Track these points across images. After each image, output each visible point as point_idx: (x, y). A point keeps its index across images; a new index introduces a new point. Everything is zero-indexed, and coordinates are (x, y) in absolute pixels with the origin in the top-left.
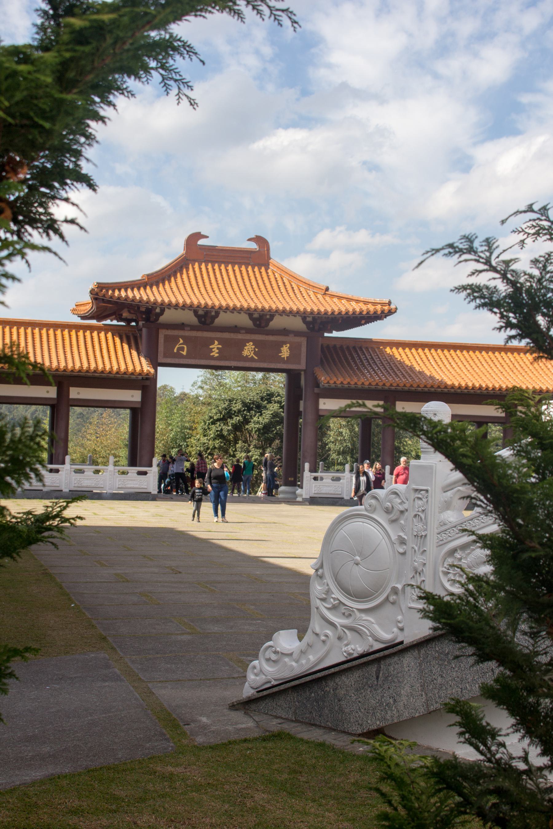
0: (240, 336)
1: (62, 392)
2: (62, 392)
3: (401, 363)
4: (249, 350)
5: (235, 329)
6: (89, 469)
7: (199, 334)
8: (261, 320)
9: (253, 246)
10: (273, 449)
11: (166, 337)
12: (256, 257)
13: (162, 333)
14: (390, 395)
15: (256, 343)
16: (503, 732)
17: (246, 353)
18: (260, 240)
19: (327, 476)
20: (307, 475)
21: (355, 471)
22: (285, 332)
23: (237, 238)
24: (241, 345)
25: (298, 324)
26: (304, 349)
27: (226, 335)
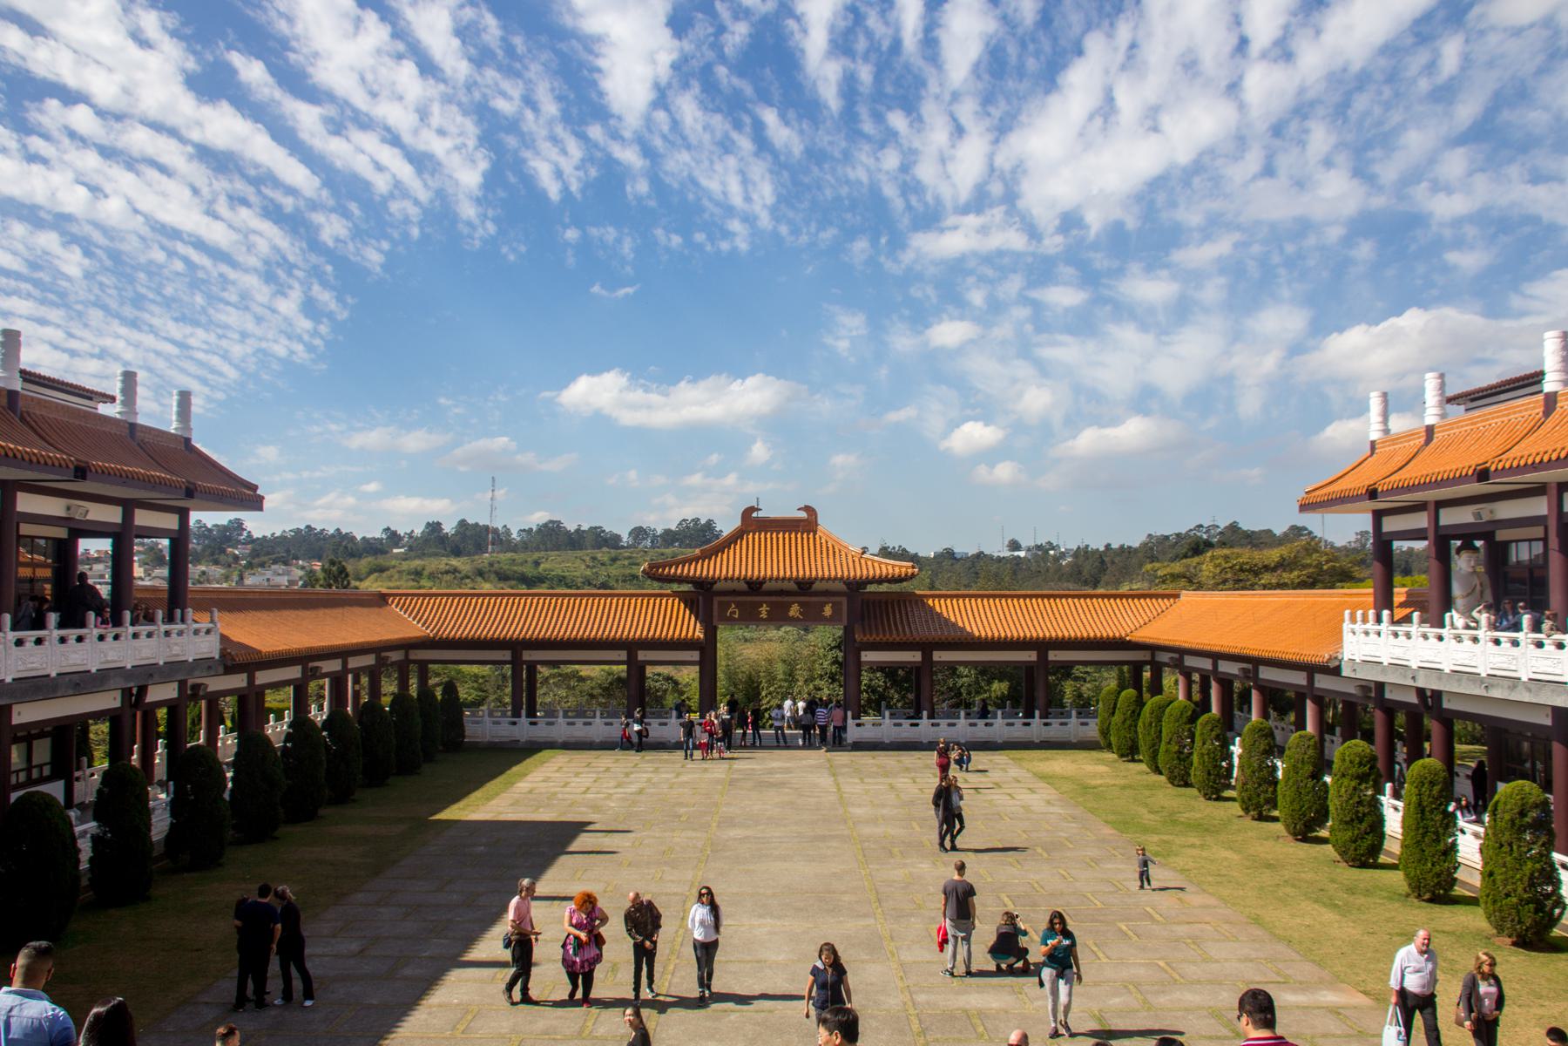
0: (786, 599)
1: (128, 516)
2: (128, 516)
3: (940, 615)
4: (794, 611)
5: (782, 593)
6: (579, 722)
7: (749, 599)
8: (804, 587)
9: (803, 515)
10: (374, 70)
11: (720, 603)
12: (806, 524)
13: (716, 600)
14: (927, 647)
15: (801, 604)
16: (1063, 987)
17: (791, 613)
18: (808, 509)
19: (1055, 722)
21: (1023, 701)
22: (826, 593)
23: (790, 510)
24: (788, 606)
25: (841, 587)
26: (845, 608)
27: (774, 599)
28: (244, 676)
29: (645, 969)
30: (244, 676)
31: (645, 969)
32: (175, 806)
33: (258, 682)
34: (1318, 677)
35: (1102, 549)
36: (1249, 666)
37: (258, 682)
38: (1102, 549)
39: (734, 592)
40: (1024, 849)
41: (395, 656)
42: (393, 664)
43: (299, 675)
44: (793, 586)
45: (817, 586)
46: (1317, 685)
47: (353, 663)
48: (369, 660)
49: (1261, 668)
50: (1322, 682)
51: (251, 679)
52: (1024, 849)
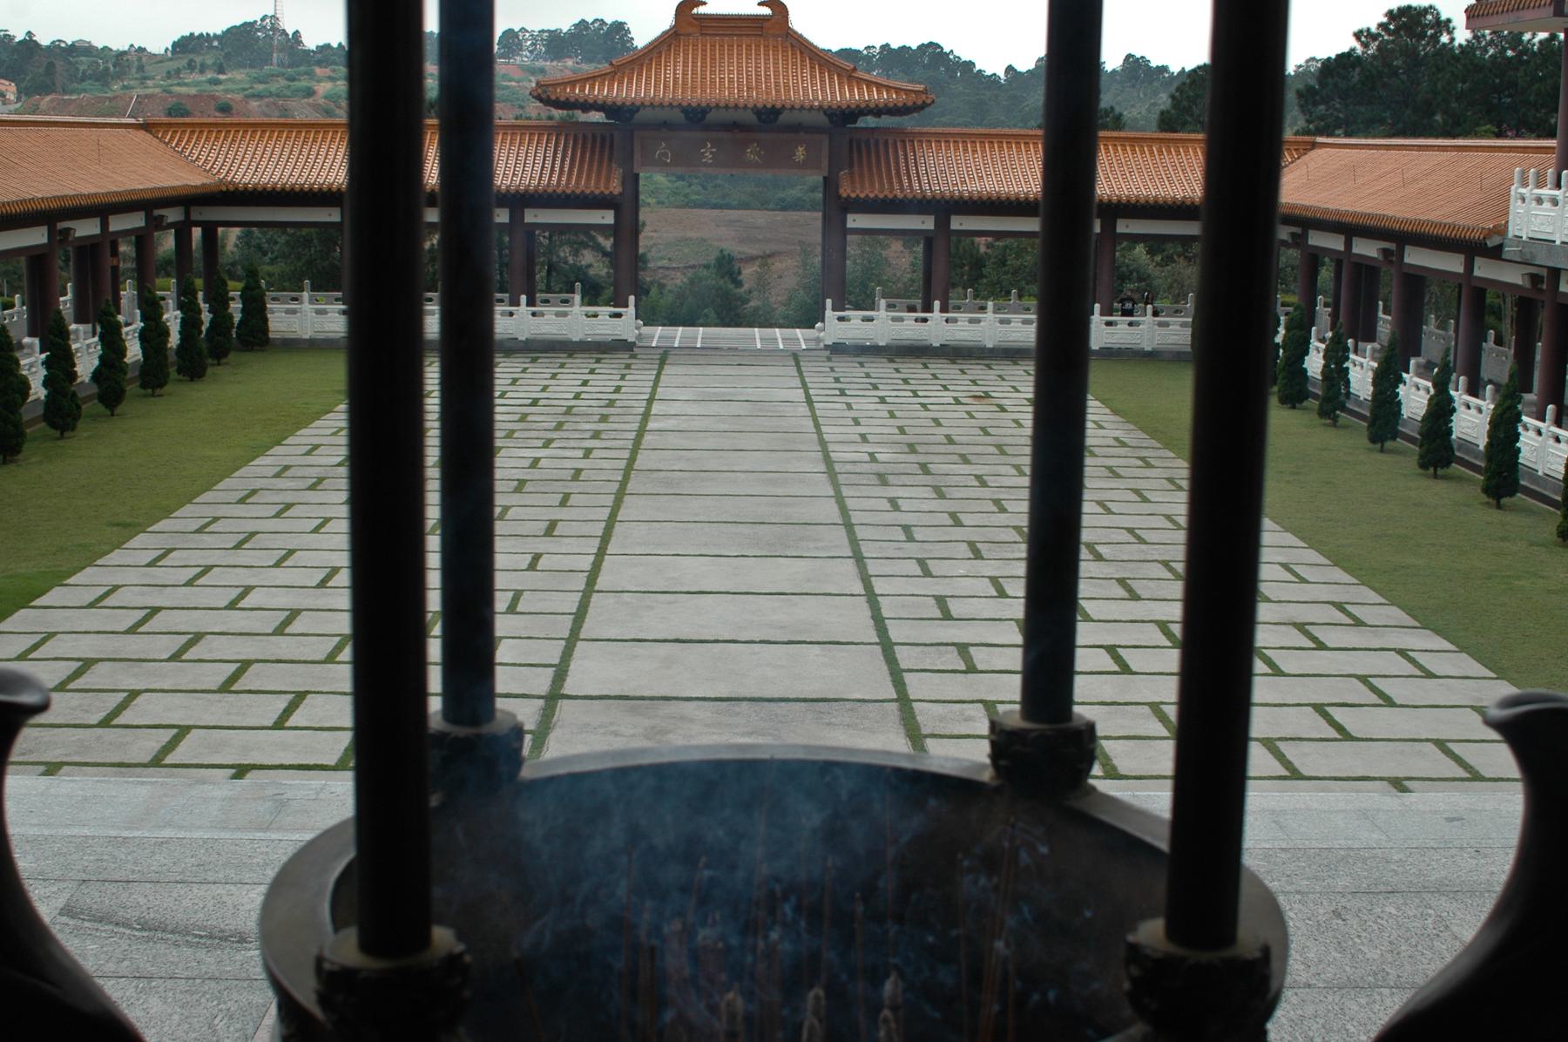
20: (830, 314)
22: (796, 128)
28: (97, 221)
29: (902, 160)
30: (97, 221)
31: (902, 160)
32: (243, 311)
33: (112, 228)
34: (1478, 261)
35: (1443, 18)
36: (1392, 246)
37: (112, 228)
38: (1443, 18)
39: (665, 125)
40: (924, 106)
41: (173, 215)
42: (170, 226)
43: (45, 240)
44: (678, 116)
45: (711, 117)
46: (1477, 273)
47: (117, 224)
48: (136, 221)
49: (1408, 249)
50: (1484, 269)
51: (105, 225)
52: (924, 106)
